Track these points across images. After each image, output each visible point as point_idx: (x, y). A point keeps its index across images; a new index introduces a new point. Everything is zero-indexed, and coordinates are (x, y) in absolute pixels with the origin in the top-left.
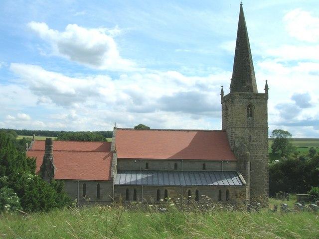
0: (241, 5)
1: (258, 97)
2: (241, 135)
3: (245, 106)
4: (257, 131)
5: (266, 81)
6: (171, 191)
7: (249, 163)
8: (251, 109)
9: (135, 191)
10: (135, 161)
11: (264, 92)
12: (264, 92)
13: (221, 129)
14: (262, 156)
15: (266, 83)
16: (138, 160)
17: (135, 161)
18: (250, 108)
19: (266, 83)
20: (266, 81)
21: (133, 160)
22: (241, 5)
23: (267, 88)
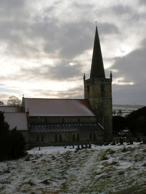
0: (97, 28)
1: (107, 81)
2: (98, 102)
3: (100, 85)
4: (107, 100)
5: (84, 74)
6: (63, 135)
7: (103, 117)
8: (103, 87)
9: (43, 136)
10: (39, 118)
11: (109, 78)
12: (109, 78)
13: (84, 98)
14: (109, 114)
15: (84, 75)
16: (41, 117)
17: (39, 118)
18: (102, 87)
19: (84, 75)
20: (84, 74)
21: (37, 117)
22: (97, 28)
23: (111, 76)
